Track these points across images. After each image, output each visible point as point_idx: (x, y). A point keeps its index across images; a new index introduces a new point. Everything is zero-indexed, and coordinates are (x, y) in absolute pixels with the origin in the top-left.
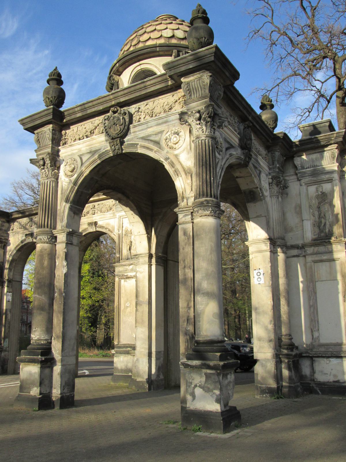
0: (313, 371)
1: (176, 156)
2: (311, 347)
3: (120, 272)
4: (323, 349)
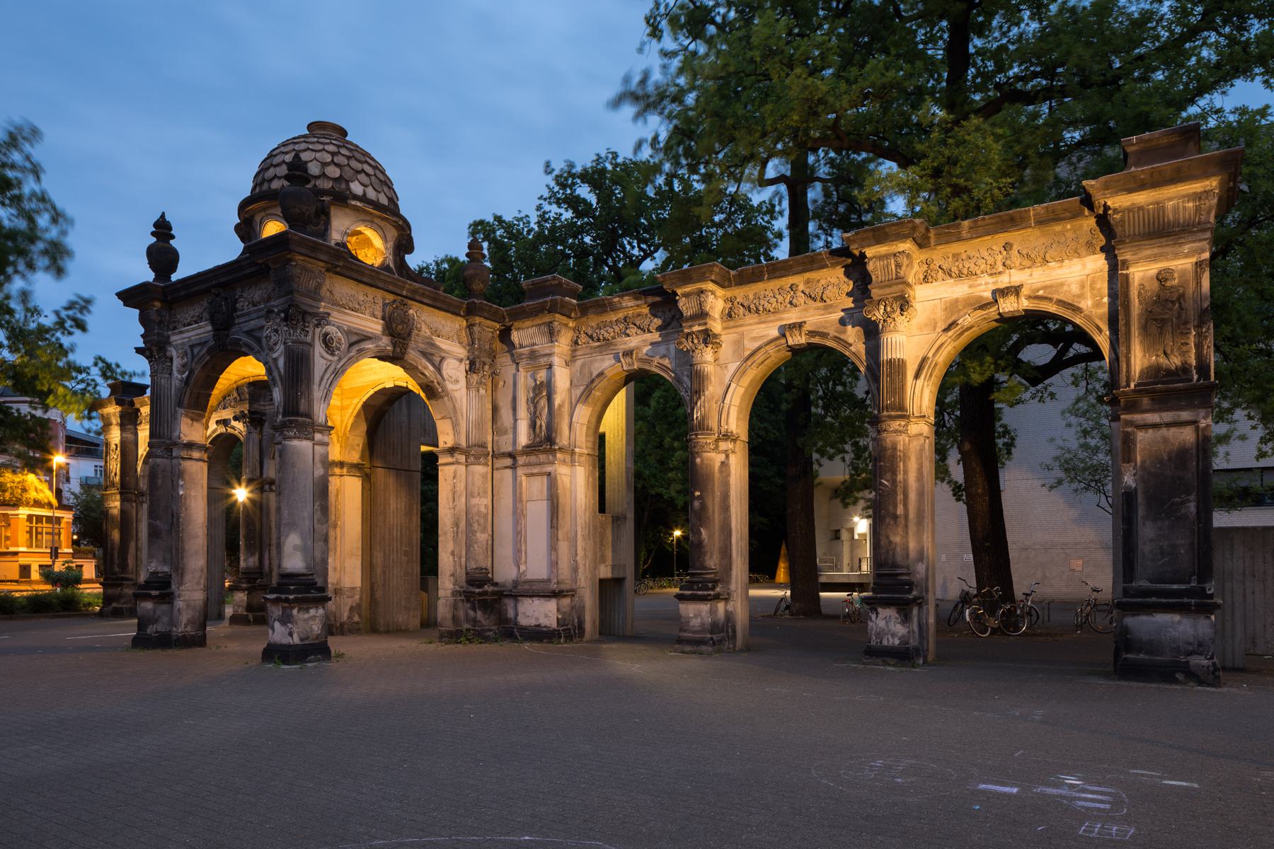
0: (517, 615)
1: (275, 360)
2: (516, 583)
4: (526, 587)
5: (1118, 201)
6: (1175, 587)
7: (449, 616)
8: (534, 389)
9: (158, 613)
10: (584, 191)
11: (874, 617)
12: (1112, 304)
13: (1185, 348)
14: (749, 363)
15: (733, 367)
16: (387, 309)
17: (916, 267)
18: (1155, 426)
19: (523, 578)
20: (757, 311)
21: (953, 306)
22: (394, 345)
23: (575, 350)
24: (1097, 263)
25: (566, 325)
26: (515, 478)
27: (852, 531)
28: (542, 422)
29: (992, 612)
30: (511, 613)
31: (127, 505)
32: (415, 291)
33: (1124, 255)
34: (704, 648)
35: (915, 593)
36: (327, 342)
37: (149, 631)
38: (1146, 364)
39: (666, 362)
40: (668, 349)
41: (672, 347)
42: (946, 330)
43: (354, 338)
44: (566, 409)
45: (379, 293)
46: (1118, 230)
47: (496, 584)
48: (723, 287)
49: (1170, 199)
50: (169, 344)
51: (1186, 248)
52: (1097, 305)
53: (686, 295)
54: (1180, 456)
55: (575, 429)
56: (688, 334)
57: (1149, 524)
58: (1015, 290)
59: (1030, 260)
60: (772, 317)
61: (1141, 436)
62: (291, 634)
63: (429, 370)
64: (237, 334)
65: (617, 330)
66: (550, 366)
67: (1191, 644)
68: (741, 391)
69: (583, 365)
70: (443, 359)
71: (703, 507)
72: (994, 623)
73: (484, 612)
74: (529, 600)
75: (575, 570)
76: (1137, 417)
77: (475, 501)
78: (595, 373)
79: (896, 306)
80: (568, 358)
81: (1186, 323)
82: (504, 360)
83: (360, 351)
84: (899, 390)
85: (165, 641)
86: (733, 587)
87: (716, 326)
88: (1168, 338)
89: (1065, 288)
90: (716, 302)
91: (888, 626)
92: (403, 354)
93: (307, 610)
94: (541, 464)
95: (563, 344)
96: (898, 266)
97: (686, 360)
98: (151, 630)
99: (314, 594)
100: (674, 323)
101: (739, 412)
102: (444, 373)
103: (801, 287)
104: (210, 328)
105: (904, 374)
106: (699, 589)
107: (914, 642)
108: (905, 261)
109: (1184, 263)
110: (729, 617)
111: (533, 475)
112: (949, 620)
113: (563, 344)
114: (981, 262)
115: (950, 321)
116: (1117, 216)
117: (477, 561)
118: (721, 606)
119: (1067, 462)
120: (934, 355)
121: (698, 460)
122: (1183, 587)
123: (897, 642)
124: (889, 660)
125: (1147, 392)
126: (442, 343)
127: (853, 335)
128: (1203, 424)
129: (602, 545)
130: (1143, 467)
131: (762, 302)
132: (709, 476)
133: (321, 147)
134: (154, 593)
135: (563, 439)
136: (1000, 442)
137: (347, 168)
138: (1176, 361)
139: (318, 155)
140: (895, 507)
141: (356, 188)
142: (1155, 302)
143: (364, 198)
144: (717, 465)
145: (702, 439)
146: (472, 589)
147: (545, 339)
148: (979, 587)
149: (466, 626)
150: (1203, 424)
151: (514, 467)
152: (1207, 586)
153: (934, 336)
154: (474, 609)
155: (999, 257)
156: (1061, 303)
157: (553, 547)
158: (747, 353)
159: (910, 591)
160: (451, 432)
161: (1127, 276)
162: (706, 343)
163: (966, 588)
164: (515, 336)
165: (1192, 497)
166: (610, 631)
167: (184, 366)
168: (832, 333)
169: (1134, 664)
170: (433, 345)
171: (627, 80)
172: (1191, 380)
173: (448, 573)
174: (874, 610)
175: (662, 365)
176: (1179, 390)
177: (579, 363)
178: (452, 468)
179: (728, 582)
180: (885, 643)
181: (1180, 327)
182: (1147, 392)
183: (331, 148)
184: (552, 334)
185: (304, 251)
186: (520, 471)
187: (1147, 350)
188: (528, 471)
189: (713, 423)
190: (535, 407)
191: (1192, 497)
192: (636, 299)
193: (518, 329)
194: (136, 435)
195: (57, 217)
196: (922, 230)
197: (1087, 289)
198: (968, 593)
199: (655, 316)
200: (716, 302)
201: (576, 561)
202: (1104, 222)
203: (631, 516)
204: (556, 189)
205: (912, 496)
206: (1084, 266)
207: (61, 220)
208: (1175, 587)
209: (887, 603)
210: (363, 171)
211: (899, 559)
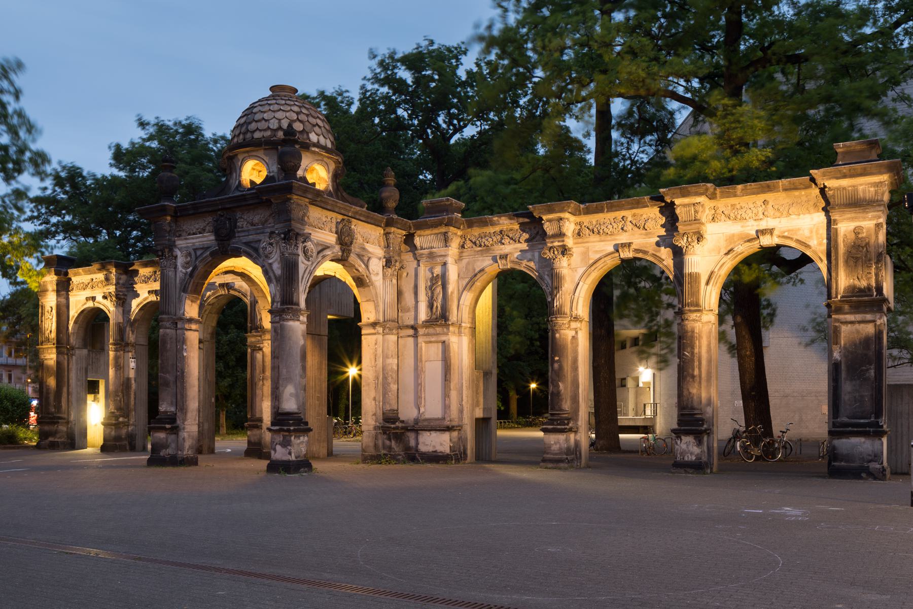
0: (417, 444)
1: (271, 264)
2: (417, 421)
3: (252, 342)
4: (425, 423)
5: (831, 183)
6: (862, 421)
7: (372, 444)
8: (432, 280)
9: (169, 440)
10: (405, 75)
11: (679, 442)
12: (829, 244)
13: (869, 276)
14: (593, 268)
15: (581, 271)
16: (341, 226)
17: (707, 211)
18: (852, 323)
19: (423, 417)
20: (599, 233)
21: (731, 238)
22: (343, 251)
23: (462, 252)
24: (820, 218)
25: (456, 234)
26: (416, 345)
27: (637, 379)
28: (438, 304)
29: (756, 444)
30: (412, 443)
31: (61, 357)
32: (356, 213)
33: (835, 216)
34: (562, 465)
35: (705, 426)
36: (305, 252)
37: (162, 454)
38: (847, 284)
39: (532, 264)
40: (533, 256)
41: (536, 254)
42: (727, 254)
43: (320, 248)
44: (455, 295)
45: (334, 215)
46: (831, 200)
47: (403, 422)
48: (574, 215)
49: (861, 185)
50: (175, 246)
51: (870, 215)
52: (820, 244)
53: (550, 221)
54: (866, 341)
55: (460, 310)
56: (551, 248)
57: (848, 383)
58: (771, 231)
59: (779, 212)
60: (609, 238)
61: (845, 329)
62: (290, 453)
63: (362, 268)
64: (234, 243)
65: (495, 239)
66: (445, 264)
67: (870, 455)
68: (586, 287)
69: (468, 263)
70: (369, 259)
71: (561, 368)
72: (756, 452)
73: (396, 442)
74: (428, 433)
75: (461, 411)
76: (842, 317)
77: (389, 361)
78: (477, 270)
79: (695, 238)
80: (457, 258)
81: (870, 260)
82: (408, 257)
83: (324, 257)
84: (696, 293)
85: (175, 461)
86: (580, 423)
87: (569, 242)
88: (860, 268)
89: (801, 232)
90: (570, 224)
91: (688, 448)
92: (348, 257)
93: (299, 437)
94: (437, 334)
95: (453, 249)
96: (696, 212)
97: (548, 266)
98: (163, 453)
99: (303, 427)
100: (538, 237)
101: (584, 301)
102: (371, 268)
103: (630, 219)
104: (213, 238)
105: (699, 283)
106: (558, 424)
107: (704, 459)
108: (701, 209)
109: (871, 225)
110: (577, 444)
111: (430, 342)
112: (727, 451)
113: (453, 249)
114: (749, 211)
115: (729, 248)
116: (831, 193)
117: (390, 405)
118: (572, 436)
119: (819, 324)
120: (719, 270)
121: (557, 335)
122: (866, 421)
123: (694, 458)
124: (688, 470)
125: (847, 302)
126: (369, 247)
127: (666, 254)
128: (878, 322)
129: (477, 393)
130: (845, 348)
131: (602, 227)
132: (564, 347)
133: (289, 108)
134: (168, 426)
135: (453, 317)
136: (765, 312)
137: (307, 123)
138: (863, 284)
139: (288, 114)
140: (693, 370)
141: (313, 137)
142: (853, 246)
143: (317, 145)
144: (570, 338)
145: (560, 321)
146: (388, 425)
147: (442, 244)
148: (747, 426)
149: (383, 452)
150: (878, 322)
151: (415, 336)
152: (880, 420)
153: (718, 257)
154: (390, 440)
155: (761, 210)
156: (798, 241)
157: (446, 395)
158: (591, 262)
159: (702, 425)
160: (374, 311)
161: (836, 229)
162: (563, 254)
163: (738, 427)
164: (417, 241)
165: (872, 367)
166: (482, 456)
167: (187, 263)
168: (651, 252)
169: (838, 468)
170: (364, 249)
171: (477, 26)
172: (872, 296)
173: (371, 414)
174: (679, 437)
175: (529, 266)
176: (865, 301)
177: (465, 262)
178: (374, 337)
179: (576, 420)
180: (686, 459)
181: (867, 262)
182: (847, 302)
183: (296, 109)
184: (446, 241)
185: (299, 193)
186: (420, 339)
187: (847, 276)
188: (428, 339)
189: (567, 310)
190: (432, 293)
191: (872, 367)
192: (511, 219)
193: (420, 236)
194: (68, 299)
195: (30, 128)
196: (712, 190)
197: (814, 234)
198: (738, 431)
199: (524, 231)
200: (570, 224)
201: (461, 405)
202: (823, 191)
203: (495, 371)
204: (378, 70)
205: (704, 363)
206: (812, 219)
207: (33, 131)
208: (862, 421)
209: (687, 433)
210: (317, 124)
211: (695, 404)
